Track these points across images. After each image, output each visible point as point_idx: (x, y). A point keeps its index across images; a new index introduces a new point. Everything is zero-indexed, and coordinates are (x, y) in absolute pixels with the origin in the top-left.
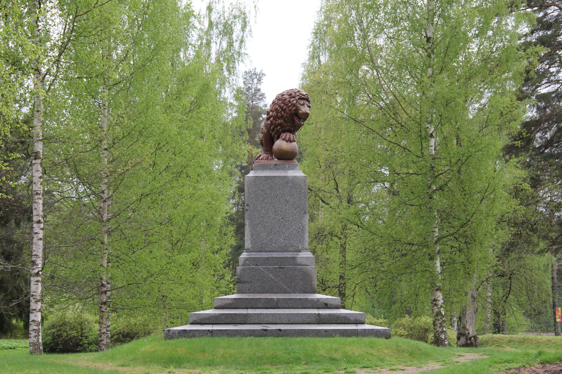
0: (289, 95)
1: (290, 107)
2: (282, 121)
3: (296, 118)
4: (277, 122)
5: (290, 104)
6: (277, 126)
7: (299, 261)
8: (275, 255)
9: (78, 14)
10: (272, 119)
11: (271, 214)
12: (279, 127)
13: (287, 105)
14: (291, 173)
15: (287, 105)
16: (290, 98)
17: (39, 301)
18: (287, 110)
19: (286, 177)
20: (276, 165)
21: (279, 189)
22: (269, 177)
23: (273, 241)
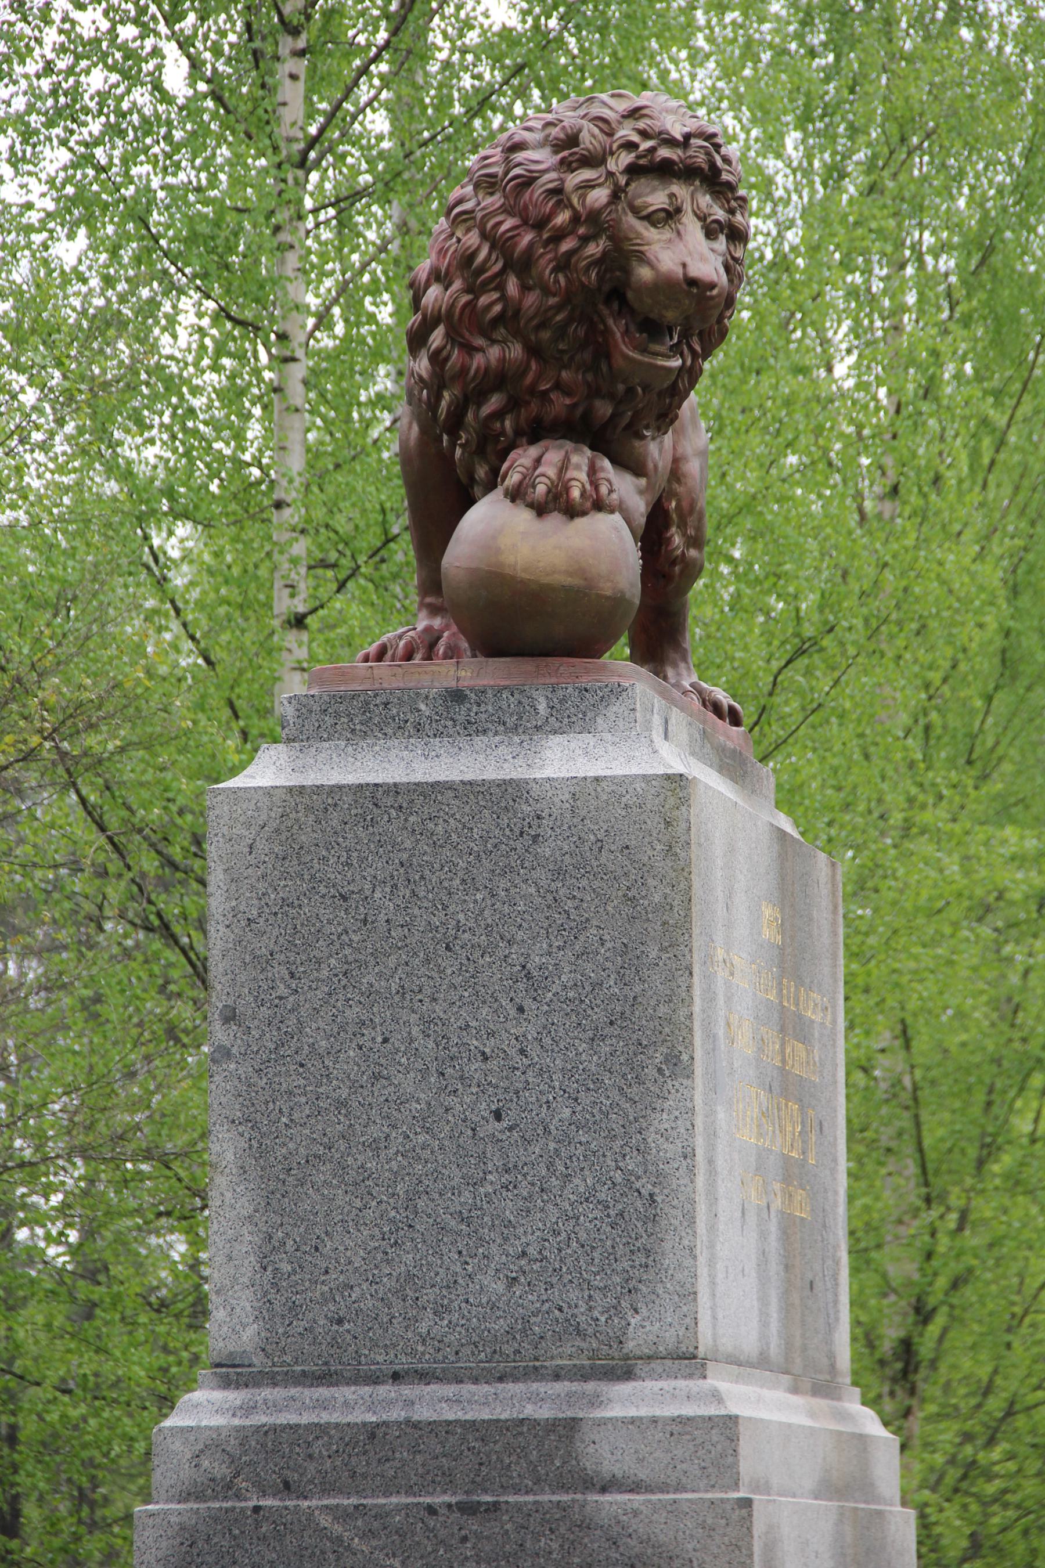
0: (558, 146)
1: (559, 236)
2: (516, 351)
3: (617, 328)
4: (478, 361)
5: (562, 218)
6: (480, 396)
7: (605, 1455)
8: (433, 1404)
10: (437, 337)
11: (408, 1083)
12: (494, 402)
13: (539, 225)
14: (561, 761)
15: (539, 225)
16: (567, 166)
17: (130, 1447)
18: (545, 266)
19: (512, 791)
20: (457, 696)
21: (469, 883)
22: (395, 789)
23: (430, 1294)
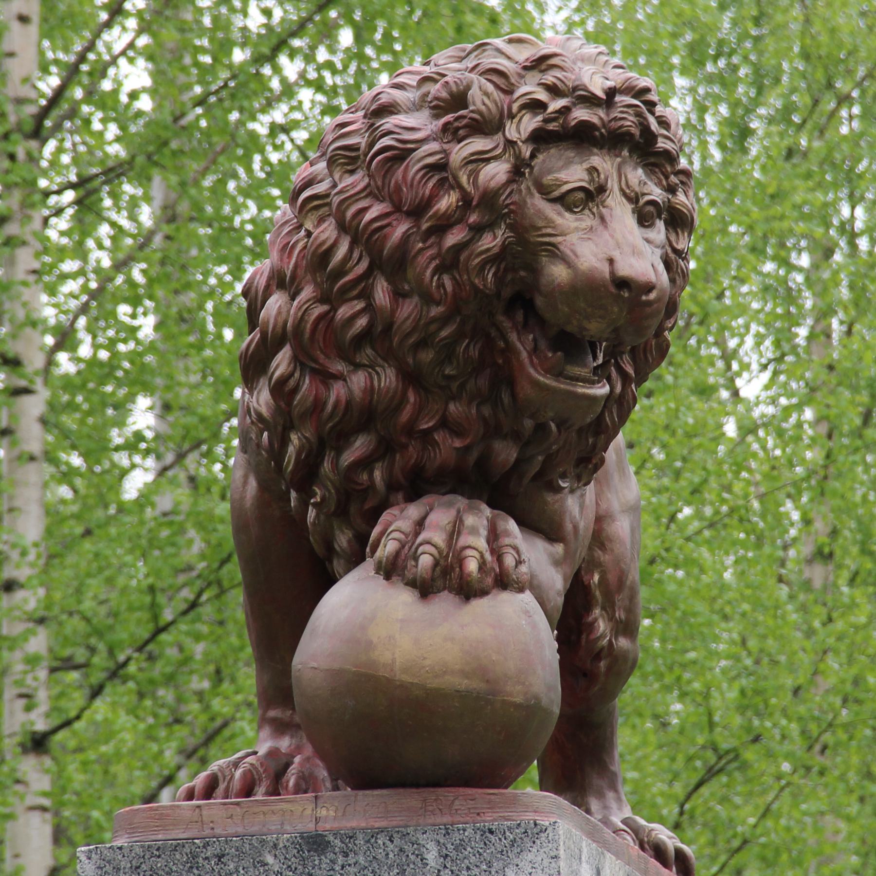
0: (439, 108)
1: (443, 226)
2: (388, 378)
3: (522, 345)
4: (337, 392)
5: (447, 202)
6: (339, 438)
9: (162, 623)
10: (281, 362)
12: (359, 446)
13: (417, 212)
15: (417, 212)
16: (452, 133)
18: (425, 265)
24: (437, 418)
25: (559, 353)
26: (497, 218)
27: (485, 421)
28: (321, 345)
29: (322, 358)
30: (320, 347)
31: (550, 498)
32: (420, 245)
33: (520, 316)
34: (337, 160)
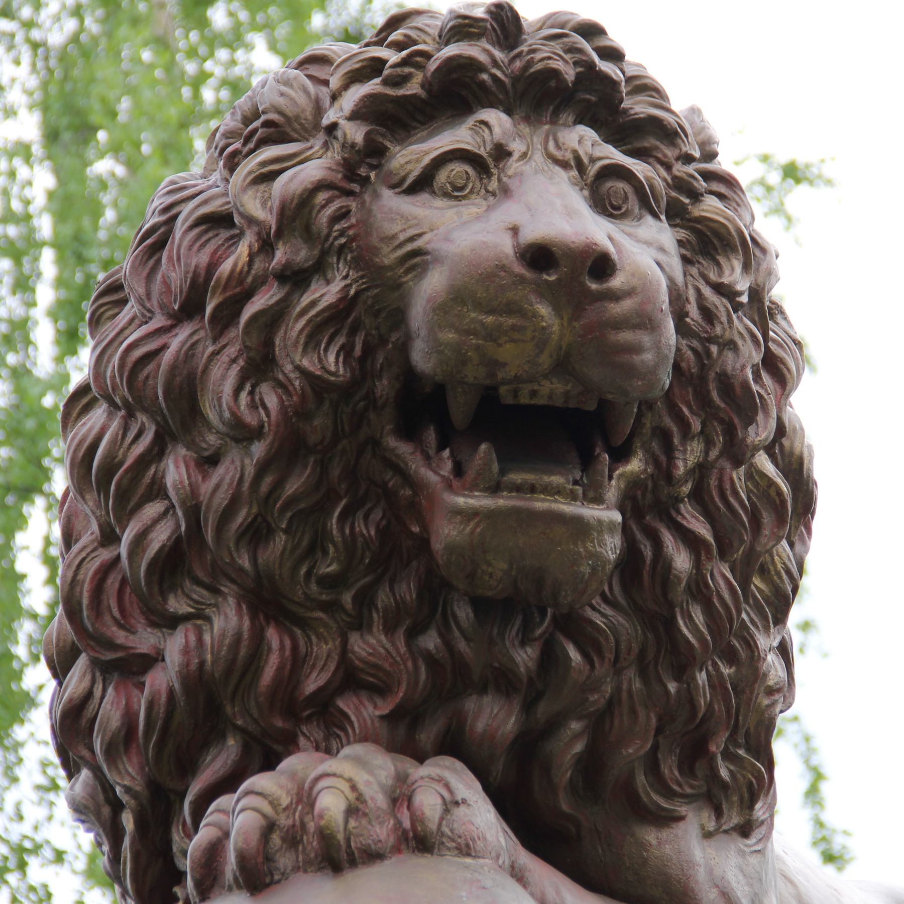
24: (332, 666)
25: (483, 447)
26: (324, 254)
27: (431, 660)
28: (116, 614)
29: (121, 637)
30: (114, 618)
31: (651, 836)
32: (210, 349)
33: (431, 436)
34: (103, 313)
